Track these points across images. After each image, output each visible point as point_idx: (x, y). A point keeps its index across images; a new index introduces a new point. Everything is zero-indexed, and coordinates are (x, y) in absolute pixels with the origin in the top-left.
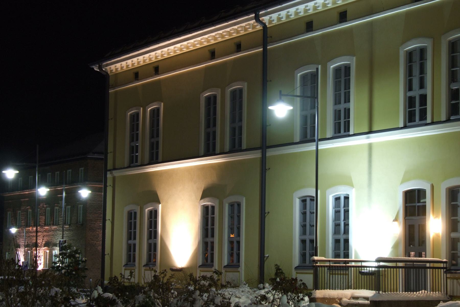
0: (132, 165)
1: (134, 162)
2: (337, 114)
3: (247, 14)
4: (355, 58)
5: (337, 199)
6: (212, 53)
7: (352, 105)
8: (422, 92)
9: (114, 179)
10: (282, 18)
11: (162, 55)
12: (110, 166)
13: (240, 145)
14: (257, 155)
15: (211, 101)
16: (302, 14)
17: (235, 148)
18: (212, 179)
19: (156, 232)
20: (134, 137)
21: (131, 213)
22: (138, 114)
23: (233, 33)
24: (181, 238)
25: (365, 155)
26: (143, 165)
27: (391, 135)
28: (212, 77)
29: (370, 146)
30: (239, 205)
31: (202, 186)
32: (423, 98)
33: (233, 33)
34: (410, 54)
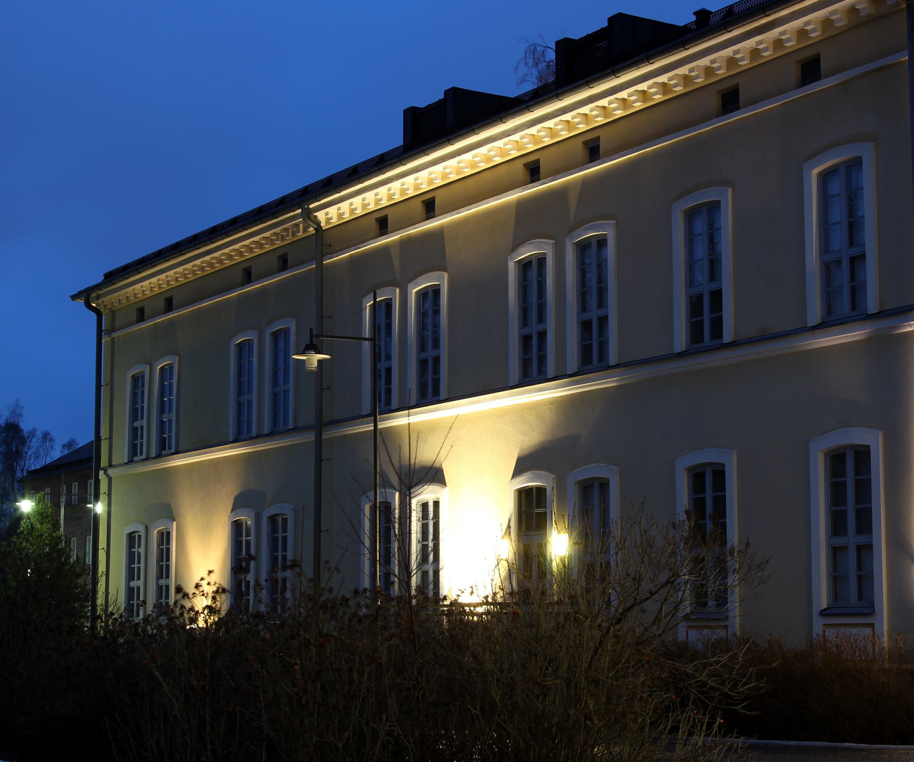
0: (135, 458)
5: (425, 506)
6: (533, 170)
10: (356, 209)
12: (104, 462)
13: (249, 431)
14: (310, 437)
16: (372, 207)
17: (591, 360)
21: (163, 533)
23: (579, 123)
27: (497, 398)
28: (529, 220)
30: (719, 474)
31: (236, 492)
33: (579, 123)
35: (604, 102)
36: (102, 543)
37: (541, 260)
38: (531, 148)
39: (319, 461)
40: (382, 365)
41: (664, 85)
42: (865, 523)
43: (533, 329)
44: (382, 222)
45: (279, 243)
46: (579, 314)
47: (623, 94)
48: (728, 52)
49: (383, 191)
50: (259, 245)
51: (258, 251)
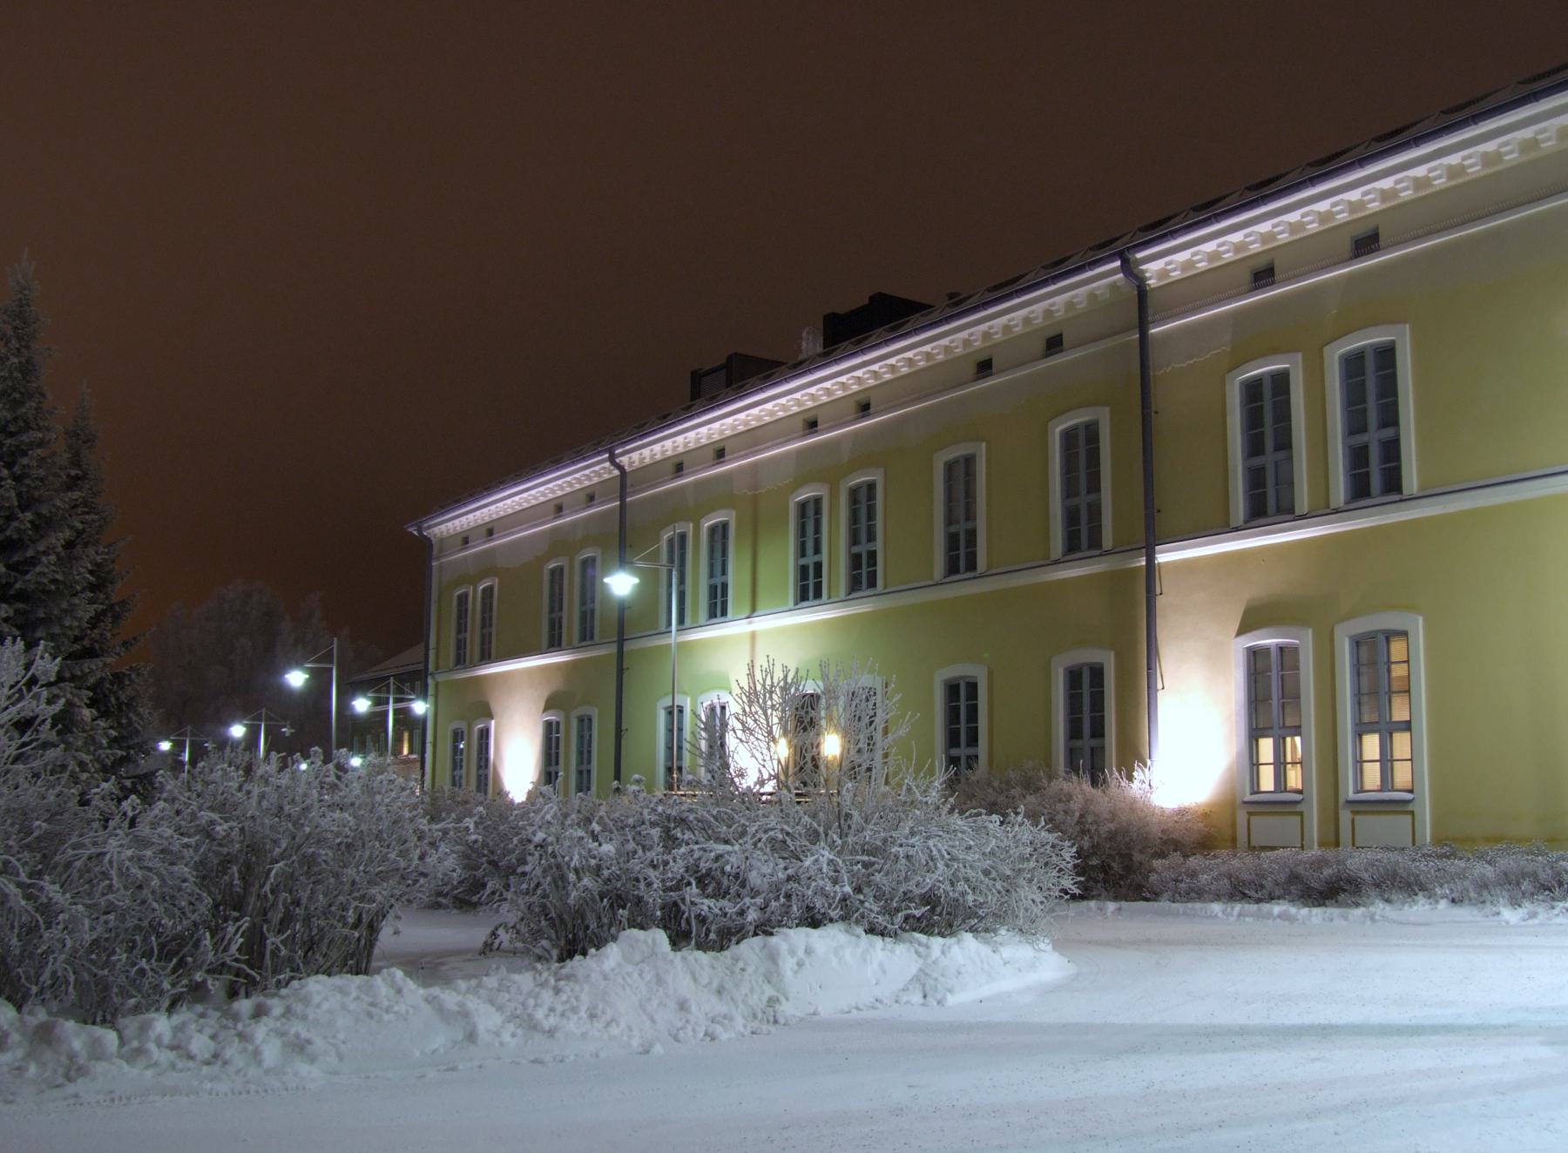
1: (461, 661)
2: (713, 590)
3: (599, 453)
4: (1300, 355)
6: (559, 509)
7: (731, 579)
8: (816, 558)
9: (437, 684)
11: (686, 444)
15: (557, 574)
16: (669, 453)
17: (587, 636)
18: (556, 685)
19: (487, 760)
20: (461, 628)
21: (958, 686)
22: (466, 595)
24: (518, 763)
25: (747, 647)
26: (474, 665)
28: (808, 467)
29: (753, 635)
31: (545, 694)
32: (818, 566)
34: (803, 506)
35: (875, 367)
36: (429, 738)
37: (871, 487)
38: (810, 404)
39: (621, 671)
40: (1374, 437)
41: (946, 347)
42: (1098, 731)
43: (961, 528)
44: (679, 467)
45: (587, 483)
46: (796, 560)
47: (892, 361)
48: (984, 327)
49: (691, 435)
50: (579, 481)
51: (568, 490)
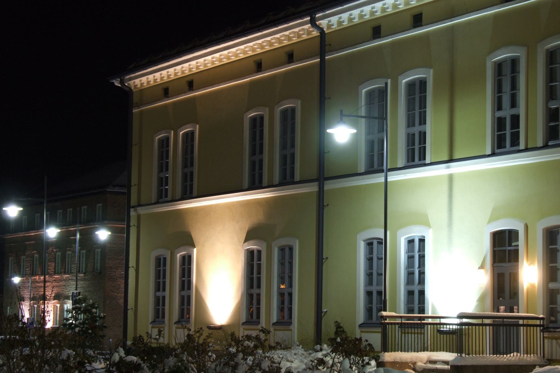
0: (160, 200)
1: (163, 197)
2: (410, 139)
3: (301, 17)
4: (432, 70)
5: (411, 242)
6: (258, 64)
7: (428, 128)
8: (514, 111)
9: (139, 217)
10: (343, 22)
11: (197, 67)
12: (133, 202)
13: (293, 176)
14: (313, 188)
15: (257, 123)
16: (367, 17)
17: (287, 179)
18: (258, 217)
19: (190, 282)
20: (163, 166)
21: (160, 259)
22: (167, 139)
23: (284, 40)
24: (220, 289)
25: (445, 188)
26: (174, 200)
27: (476, 163)
28: (258, 94)
29: (451, 178)
30: (291, 249)
31: (246, 226)
32: (515, 119)
33: (284, 40)
34: (499, 66)
